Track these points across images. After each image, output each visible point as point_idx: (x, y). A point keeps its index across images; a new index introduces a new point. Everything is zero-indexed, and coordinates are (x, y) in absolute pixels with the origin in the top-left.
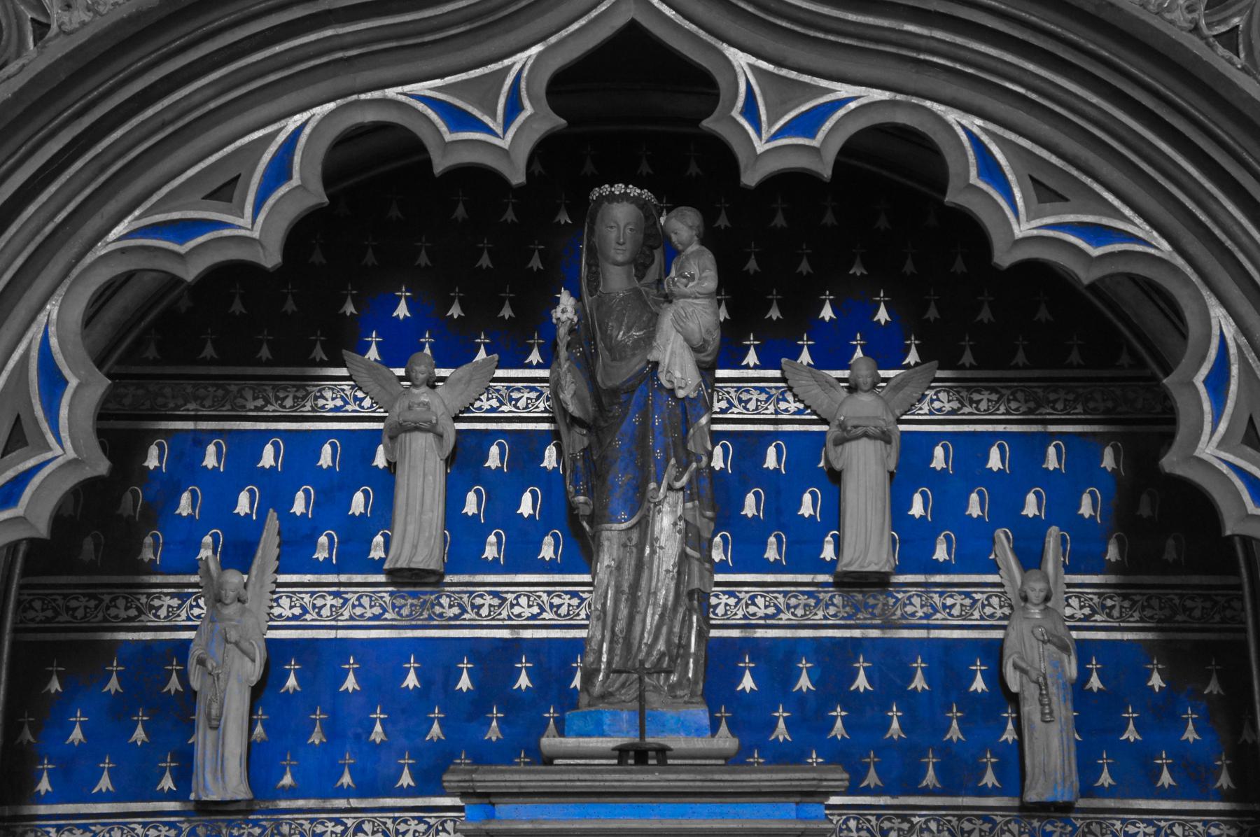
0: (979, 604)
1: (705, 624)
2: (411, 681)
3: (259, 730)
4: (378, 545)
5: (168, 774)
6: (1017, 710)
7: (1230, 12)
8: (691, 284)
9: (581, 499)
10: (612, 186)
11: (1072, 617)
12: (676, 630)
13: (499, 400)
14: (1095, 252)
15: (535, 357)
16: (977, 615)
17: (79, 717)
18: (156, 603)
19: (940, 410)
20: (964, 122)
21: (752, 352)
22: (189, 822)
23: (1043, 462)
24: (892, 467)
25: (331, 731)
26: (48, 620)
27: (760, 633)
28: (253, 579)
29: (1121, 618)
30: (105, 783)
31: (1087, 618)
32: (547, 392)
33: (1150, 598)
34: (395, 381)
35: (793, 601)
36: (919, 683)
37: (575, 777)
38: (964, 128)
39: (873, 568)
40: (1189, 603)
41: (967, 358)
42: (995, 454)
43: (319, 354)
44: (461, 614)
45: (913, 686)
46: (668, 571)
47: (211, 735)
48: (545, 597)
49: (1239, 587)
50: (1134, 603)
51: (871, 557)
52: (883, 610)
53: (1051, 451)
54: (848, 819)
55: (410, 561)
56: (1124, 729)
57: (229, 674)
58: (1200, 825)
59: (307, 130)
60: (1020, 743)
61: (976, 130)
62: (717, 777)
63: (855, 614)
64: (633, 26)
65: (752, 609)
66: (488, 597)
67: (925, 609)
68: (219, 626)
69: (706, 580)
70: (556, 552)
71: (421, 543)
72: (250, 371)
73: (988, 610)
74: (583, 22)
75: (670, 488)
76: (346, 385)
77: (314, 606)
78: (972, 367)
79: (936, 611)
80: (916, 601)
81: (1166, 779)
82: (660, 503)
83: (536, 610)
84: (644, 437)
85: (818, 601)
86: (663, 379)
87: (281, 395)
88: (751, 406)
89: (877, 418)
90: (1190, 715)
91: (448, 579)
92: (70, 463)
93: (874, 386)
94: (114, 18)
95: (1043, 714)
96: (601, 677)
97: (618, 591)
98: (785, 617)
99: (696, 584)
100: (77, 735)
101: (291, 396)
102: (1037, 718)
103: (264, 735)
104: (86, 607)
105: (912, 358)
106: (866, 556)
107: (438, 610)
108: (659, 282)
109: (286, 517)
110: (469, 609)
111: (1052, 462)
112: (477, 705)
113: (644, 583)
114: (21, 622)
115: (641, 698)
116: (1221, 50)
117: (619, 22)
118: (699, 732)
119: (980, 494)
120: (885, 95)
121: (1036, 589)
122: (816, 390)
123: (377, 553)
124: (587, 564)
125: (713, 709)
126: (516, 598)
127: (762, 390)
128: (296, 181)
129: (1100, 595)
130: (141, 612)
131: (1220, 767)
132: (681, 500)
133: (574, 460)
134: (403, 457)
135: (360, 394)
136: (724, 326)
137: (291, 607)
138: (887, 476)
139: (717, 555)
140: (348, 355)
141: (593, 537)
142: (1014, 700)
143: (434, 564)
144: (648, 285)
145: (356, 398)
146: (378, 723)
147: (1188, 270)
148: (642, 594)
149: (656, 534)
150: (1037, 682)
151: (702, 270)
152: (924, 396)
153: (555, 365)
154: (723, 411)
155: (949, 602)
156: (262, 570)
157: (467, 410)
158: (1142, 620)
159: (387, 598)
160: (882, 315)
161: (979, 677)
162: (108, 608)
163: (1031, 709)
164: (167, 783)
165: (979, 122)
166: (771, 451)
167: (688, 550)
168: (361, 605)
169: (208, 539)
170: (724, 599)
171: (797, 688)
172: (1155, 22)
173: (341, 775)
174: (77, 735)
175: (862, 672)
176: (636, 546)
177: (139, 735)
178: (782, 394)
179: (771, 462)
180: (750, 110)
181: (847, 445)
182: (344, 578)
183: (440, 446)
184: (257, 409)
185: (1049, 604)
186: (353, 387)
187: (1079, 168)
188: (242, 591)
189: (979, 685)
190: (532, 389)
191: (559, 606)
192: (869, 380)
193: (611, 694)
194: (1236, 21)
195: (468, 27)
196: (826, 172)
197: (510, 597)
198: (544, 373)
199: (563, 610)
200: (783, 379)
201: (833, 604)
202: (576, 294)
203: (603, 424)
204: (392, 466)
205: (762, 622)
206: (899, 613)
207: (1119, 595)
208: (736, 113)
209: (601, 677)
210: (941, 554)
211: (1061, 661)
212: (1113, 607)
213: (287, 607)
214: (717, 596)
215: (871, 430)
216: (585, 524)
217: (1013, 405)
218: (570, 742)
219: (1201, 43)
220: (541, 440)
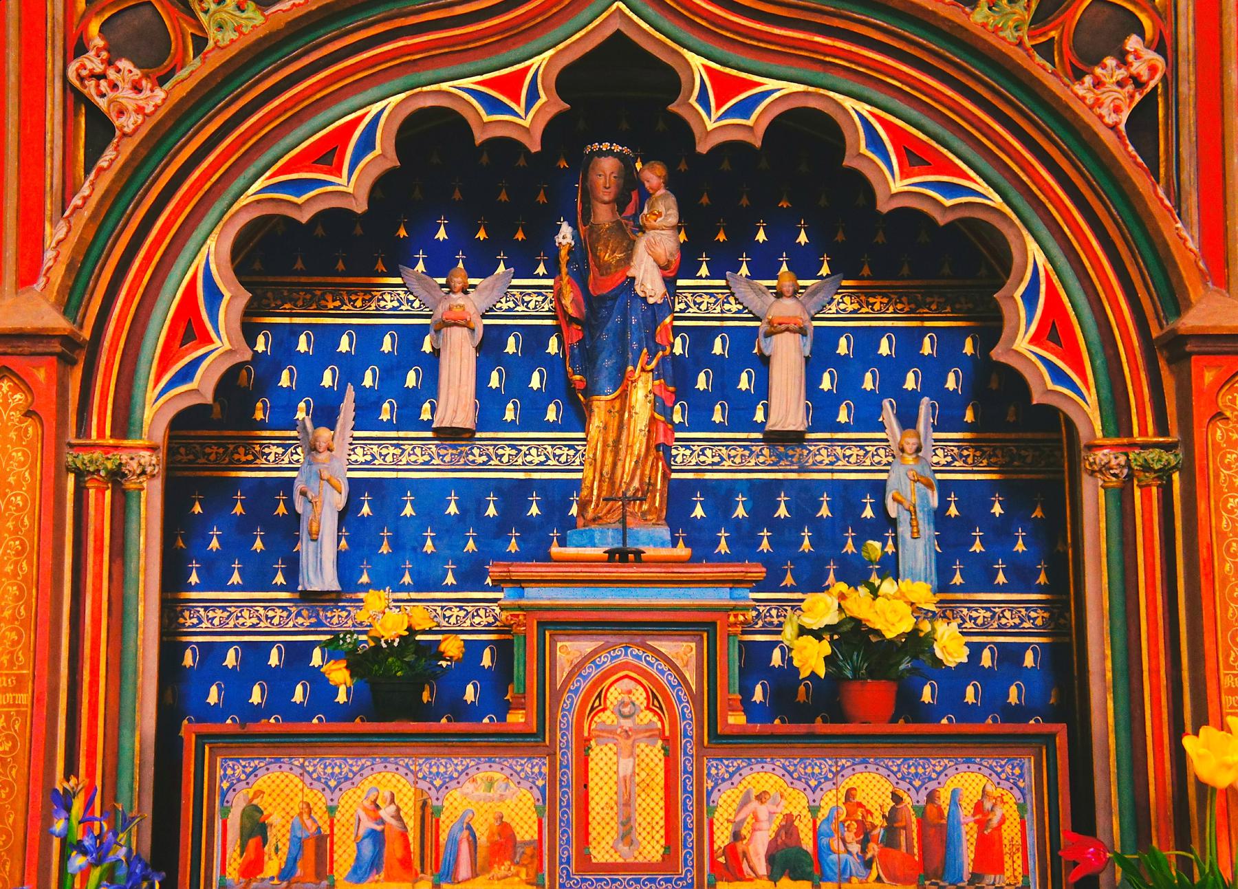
0: (870, 454)
1: (668, 469)
2: (453, 509)
3: (343, 542)
4: (426, 409)
5: (279, 573)
6: (895, 531)
7: (1049, 26)
8: (659, 219)
9: (578, 377)
10: (600, 144)
11: (938, 463)
12: (647, 472)
13: (514, 303)
14: (948, 203)
15: (541, 270)
16: (868, 462)
17: (215, 531)
18: (267, 450)
19: (844, 310)
20: (856, 108)
21: (704, 267)
22: (297, 606)
23: (921, 349)
24: (807, 353)
25: (395, 544)
26: (190, 461)
27: (708, 476)
28: (337, 434)
29: (973, 464)
30: (236, 578)
31: (948, 464)
32: (550, 296)
33: (995, 449)
34: (438, 288)
35: (733, 453)
36: (825, 511)
37: (579, 569)
38: (857, 112)
39: (791, 428)
40: (1023, 453)
41: (866, 271)
42: (884, 343)
43: (380, 267)
44: (489, 461)
45: (819, 514)
46: (641, 430)
47: (312, 545)
48: (549, 449)
49: (1060, 440)
50: (984, 453)
51: (791, 419)
52: (799, 459)
53: (927, 341)
54: (770, 609)
55: (452, 422)
56: (973, 544)
57: (323, 502)
58: (1023, 610)
59: (386, 114)
60: (896, 554)
61: (866, 114)
62: (676, 570)
63: (779, 462)
64: (618, 32)
65: (702, 458)
66: (507, 449)
67: (830, 458)
68: (315, 468)
69: (669, 437)
70: (557, 416)
71: (459, 409)
72: (330, 279)
73: (877, 459)
74: (582, 33)
75: (643, 370)
76: (401, 291)
77: (381, 455)
78: (869, 278)
79: (838, 459)
80: (824, 452)
81: (1001, 579)
82: (635, 381)
83: (543, 458)
84: (624, 332)
85: (752, 452)
86: (638, 290)
87: (353, 298)
88: (703, 307)
89: (796, 317)
90: (1020, 533)
91: (478, 435)
92: (227, 352)
93: (795, 292)
94: (254, 38)
95: (912, 532)
96: (592, 506)
97: (605, 444)
98: (727, 464)
99: (661, 440)
100: (215, 544)
101: (360, 298)
102: (908, 535)
103: (347, 547)
104: (217, 453)
105: (825, 270)
106: (786, 419)
107: (471, 458)
108: (635, 216)
109: (359, 389)
110: (494, 457)
111: (927, 349)
112: (500, 528)
113: (624, 438)
114: (172, 463)
115: (623, 521)
116: (1038, 59)
117: (608, 32)
118: (663, 545)
119: (873, 373)
120: (801, 88)
121: (910, 443)
122: (751, 295)
123: (425, 416)
124: (583, 425)
125: (673, 531)
126: (529, 450)
127: (711, 295)
128: (378, 151)
129: (958, 447)
130: (256, 458)
131: (1040, 569)
132: (651, 379)
133: (572, 348)
134: (445, 344)
135: (411, 298)
136: (683, 247)
137: (364, 455)
138: (803, 359)
139: (677, 418)
140: (405, 269)
141: (586, 405)
142: (893, 523)
143: (469, 424)
144: (627, 219)
145: (408, 301)
146: (429, 540)
147: (1013, 216)
148: (623, 447)
149: (633, 403)
150: (908, 510)
151: (667, 210)
152: (833, 300)
153: (558, 277)
154: (682, 311)
155: (848, 453)
156: (344, 427)
157: (491, 310)
158: (988, 466)
159: (434, 449)
160: (803, 238)
161: (868, 507)
162: (232, 453)
163: (904, 530)
164: (280, 579)
165: (868, 107)
166: (718, 341)
167: (656, 415)
168: (414, 454)
169: (302, 405)
170: (682, 450)
171: (735, 515)
172: (992, 39)
173: (403, 576)
174: (215, 544)
175: (783, 505)
176: (618, 412)
177: (258, 545)
178: (726, 298)
179: (717, 349)
180: (703, 99)
181: (774, 337)
182: (402, 434)
183: (473, 338)
184: (336, 308)
185: (920, 454)
186: (406, 292)
187: (938, 142)
188: (331, 443)
189: (868, 513)
190: (539, 294)
191: (560, 456)
192: (791, 289)
193: (600, 518)
194: (1053, 33)
195: (500, 37)
196: (758, 144)
197: (524, 449)
198: (550, 282)
199: (563, 459)
200: (727, 287)
201: (762, 455)
202: (574, 225)
203: (593, 322)
204: (436, 352)
205: (710, 467)
206: (811, 461)
207: (972, 447)
208: (692, 101)
209: (592, 506)
210: (843, 417)
211: (926, 494)
212: (969, 455)
213: (361, 454)
214: (676, 448)
215: (792, 326)
216: (580, 396)
217: (899, 306)
218: (571, 551)
219: (1024, 54)
220: (545, 332)
